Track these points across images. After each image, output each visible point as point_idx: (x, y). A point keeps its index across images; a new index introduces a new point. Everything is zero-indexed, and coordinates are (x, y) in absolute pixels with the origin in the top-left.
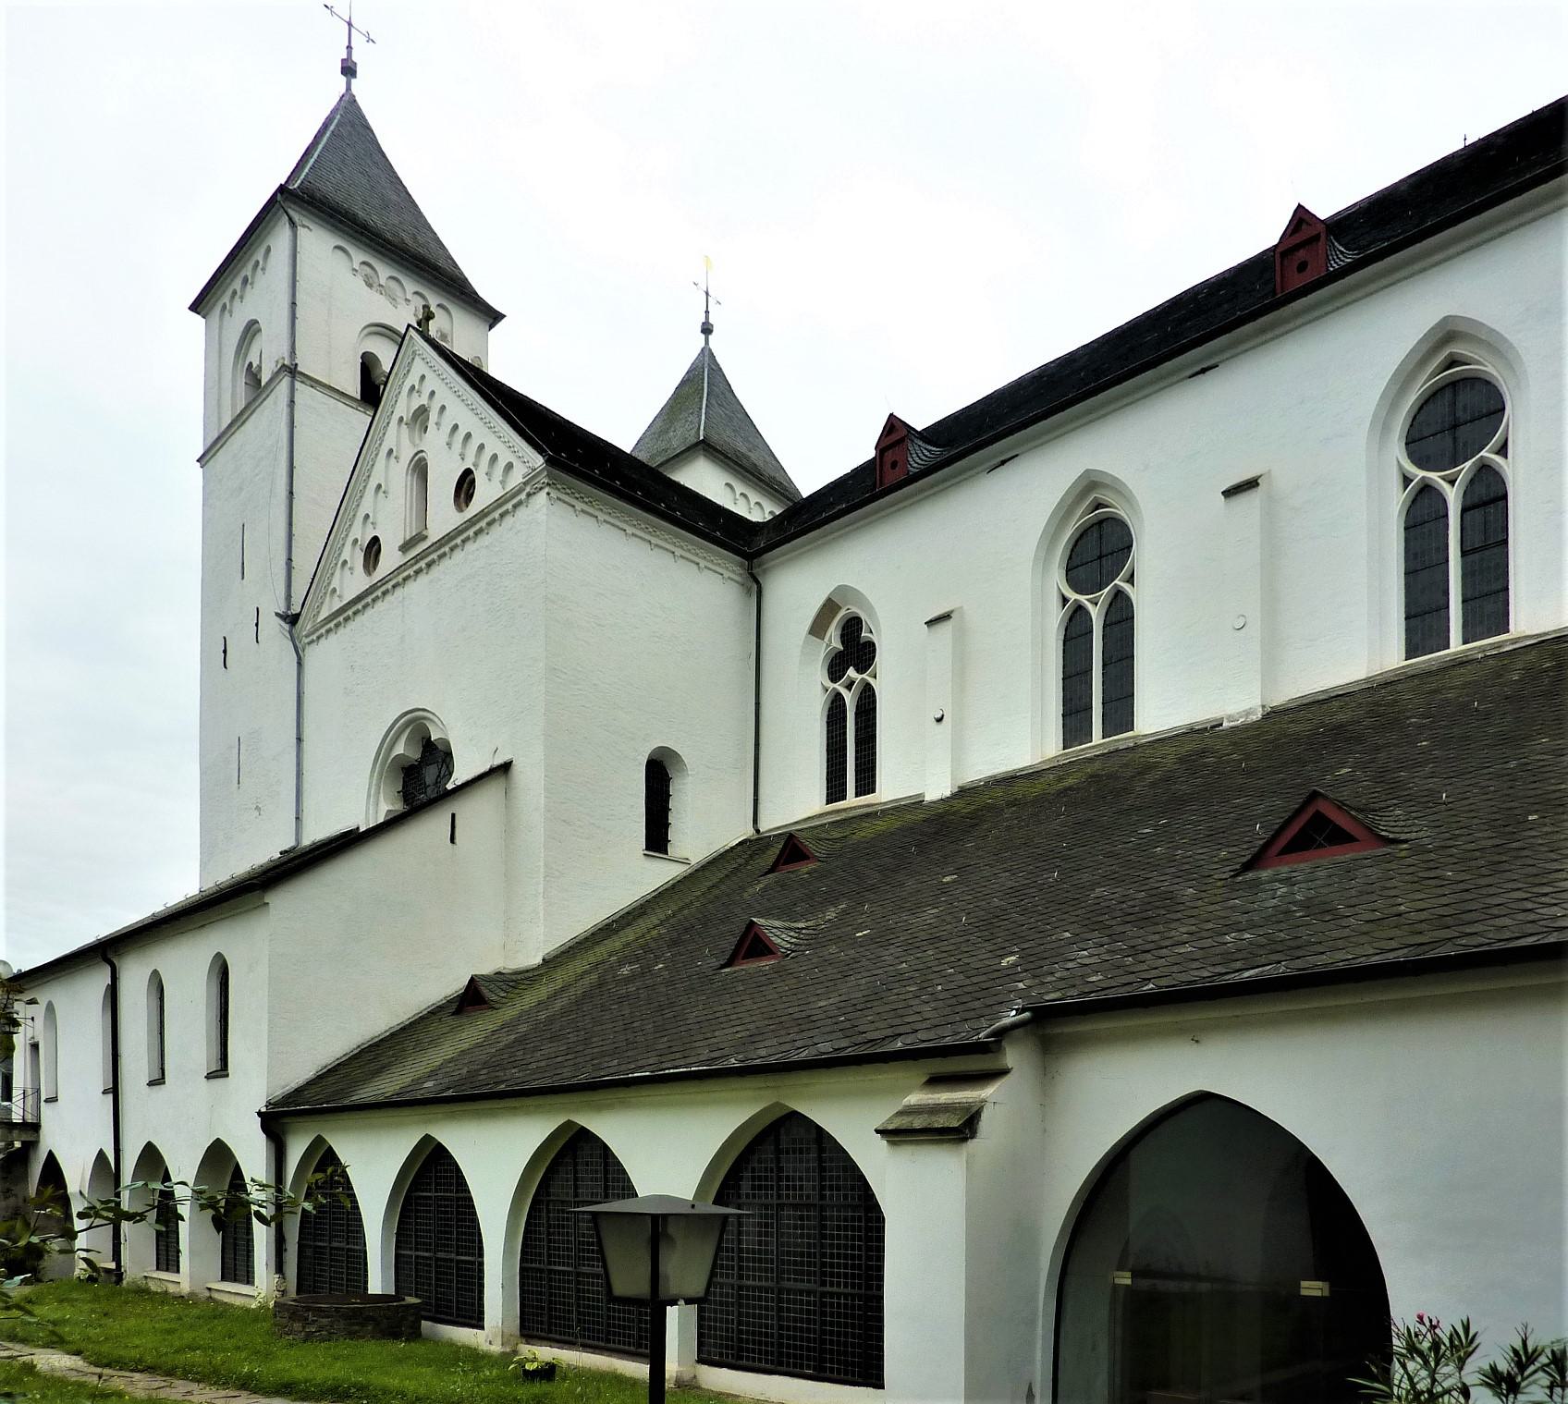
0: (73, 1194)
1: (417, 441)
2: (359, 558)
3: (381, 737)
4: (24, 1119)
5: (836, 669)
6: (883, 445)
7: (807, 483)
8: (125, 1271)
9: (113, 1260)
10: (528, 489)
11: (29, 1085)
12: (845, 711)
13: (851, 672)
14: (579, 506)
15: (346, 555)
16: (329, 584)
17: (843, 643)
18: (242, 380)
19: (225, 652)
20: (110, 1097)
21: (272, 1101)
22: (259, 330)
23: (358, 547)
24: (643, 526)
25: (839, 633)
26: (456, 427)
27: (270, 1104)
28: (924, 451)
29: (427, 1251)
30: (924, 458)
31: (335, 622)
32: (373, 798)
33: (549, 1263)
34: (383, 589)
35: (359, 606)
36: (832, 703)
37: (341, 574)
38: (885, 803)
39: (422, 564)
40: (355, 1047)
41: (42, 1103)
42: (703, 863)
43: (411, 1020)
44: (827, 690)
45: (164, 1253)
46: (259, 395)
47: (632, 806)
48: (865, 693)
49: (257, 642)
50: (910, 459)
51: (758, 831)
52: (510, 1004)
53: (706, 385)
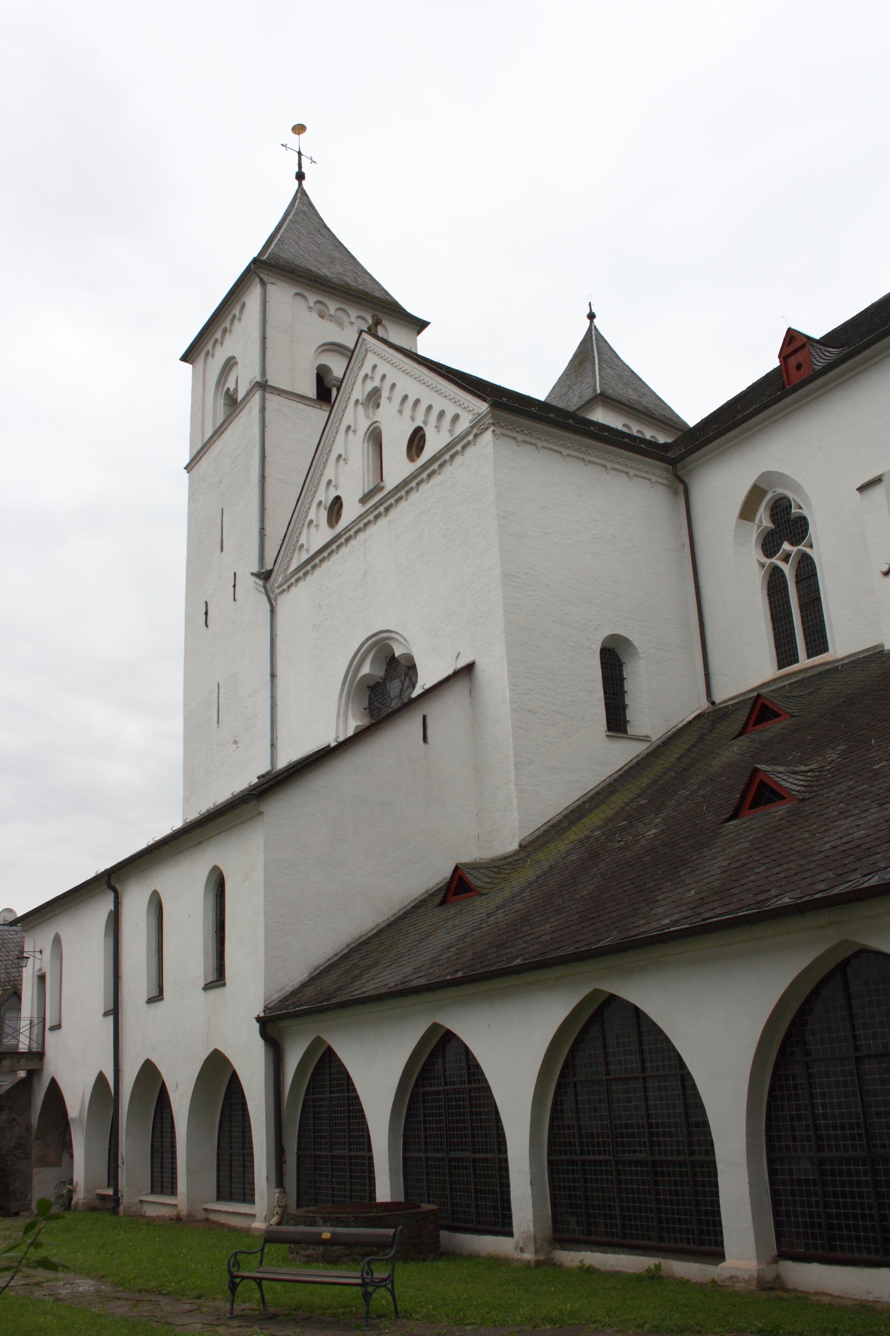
0: (74, 1119)
1: (371, 415)
2: (324, 514)
3: (349, 661)
4: (29, 1050)
5: (769, 545)
6: (783, 355)
7: (692, 415)
8: (122, 1196)
9: (109, 1185)
10: (475, 431)
11: (35, 1015)
12: (785, 582)
13: (786, 546)
14: (520, 437)
15: (312, 515)
16: (297, 541)
17: (773, 522)
18: (221, 402)
19: (206, 614)
20: (111, 1019)
21: (269, 1006)
22: (236, 363)
23: (322, 508)
24: (577, 447)
25: (768, 513)
26: (405, 397)
27: (268, 1008)
28: (825, 352)
29: (438, 1151)
30: (826, 358)
31: (303, 571)
32: (342, 715)
33: (582, 1153)
34: (347, 535)
35: (325, 554)
36: (771, 576)
37: (308, 533)
38: (842, 659)
39: (381, 509)
40: (345, 946)
41: (47, 1032)
42: (664, 739)
43: (396, 916)
44: (764, 566)
45: (159, 1175)
46: (234, 411)
47: (591, 692)
48: (800, 570)
49: (235, 600)
50: (813, 360)
51: (713, 703)
52: (498, 888)
53: (596, 354)
